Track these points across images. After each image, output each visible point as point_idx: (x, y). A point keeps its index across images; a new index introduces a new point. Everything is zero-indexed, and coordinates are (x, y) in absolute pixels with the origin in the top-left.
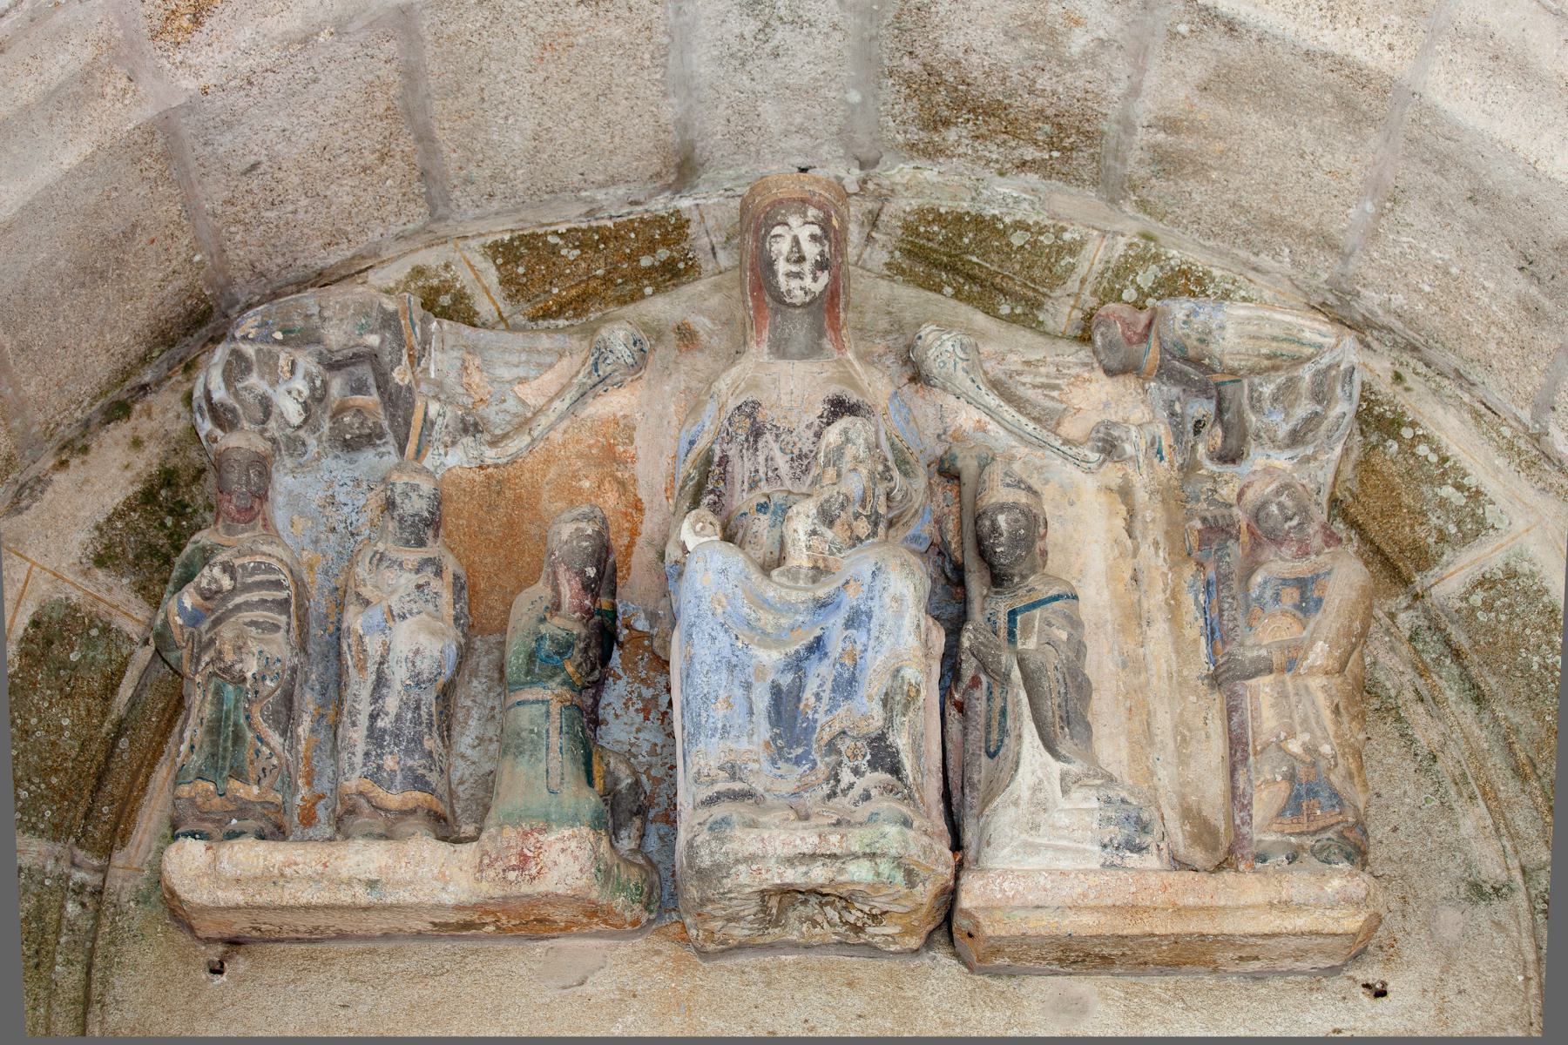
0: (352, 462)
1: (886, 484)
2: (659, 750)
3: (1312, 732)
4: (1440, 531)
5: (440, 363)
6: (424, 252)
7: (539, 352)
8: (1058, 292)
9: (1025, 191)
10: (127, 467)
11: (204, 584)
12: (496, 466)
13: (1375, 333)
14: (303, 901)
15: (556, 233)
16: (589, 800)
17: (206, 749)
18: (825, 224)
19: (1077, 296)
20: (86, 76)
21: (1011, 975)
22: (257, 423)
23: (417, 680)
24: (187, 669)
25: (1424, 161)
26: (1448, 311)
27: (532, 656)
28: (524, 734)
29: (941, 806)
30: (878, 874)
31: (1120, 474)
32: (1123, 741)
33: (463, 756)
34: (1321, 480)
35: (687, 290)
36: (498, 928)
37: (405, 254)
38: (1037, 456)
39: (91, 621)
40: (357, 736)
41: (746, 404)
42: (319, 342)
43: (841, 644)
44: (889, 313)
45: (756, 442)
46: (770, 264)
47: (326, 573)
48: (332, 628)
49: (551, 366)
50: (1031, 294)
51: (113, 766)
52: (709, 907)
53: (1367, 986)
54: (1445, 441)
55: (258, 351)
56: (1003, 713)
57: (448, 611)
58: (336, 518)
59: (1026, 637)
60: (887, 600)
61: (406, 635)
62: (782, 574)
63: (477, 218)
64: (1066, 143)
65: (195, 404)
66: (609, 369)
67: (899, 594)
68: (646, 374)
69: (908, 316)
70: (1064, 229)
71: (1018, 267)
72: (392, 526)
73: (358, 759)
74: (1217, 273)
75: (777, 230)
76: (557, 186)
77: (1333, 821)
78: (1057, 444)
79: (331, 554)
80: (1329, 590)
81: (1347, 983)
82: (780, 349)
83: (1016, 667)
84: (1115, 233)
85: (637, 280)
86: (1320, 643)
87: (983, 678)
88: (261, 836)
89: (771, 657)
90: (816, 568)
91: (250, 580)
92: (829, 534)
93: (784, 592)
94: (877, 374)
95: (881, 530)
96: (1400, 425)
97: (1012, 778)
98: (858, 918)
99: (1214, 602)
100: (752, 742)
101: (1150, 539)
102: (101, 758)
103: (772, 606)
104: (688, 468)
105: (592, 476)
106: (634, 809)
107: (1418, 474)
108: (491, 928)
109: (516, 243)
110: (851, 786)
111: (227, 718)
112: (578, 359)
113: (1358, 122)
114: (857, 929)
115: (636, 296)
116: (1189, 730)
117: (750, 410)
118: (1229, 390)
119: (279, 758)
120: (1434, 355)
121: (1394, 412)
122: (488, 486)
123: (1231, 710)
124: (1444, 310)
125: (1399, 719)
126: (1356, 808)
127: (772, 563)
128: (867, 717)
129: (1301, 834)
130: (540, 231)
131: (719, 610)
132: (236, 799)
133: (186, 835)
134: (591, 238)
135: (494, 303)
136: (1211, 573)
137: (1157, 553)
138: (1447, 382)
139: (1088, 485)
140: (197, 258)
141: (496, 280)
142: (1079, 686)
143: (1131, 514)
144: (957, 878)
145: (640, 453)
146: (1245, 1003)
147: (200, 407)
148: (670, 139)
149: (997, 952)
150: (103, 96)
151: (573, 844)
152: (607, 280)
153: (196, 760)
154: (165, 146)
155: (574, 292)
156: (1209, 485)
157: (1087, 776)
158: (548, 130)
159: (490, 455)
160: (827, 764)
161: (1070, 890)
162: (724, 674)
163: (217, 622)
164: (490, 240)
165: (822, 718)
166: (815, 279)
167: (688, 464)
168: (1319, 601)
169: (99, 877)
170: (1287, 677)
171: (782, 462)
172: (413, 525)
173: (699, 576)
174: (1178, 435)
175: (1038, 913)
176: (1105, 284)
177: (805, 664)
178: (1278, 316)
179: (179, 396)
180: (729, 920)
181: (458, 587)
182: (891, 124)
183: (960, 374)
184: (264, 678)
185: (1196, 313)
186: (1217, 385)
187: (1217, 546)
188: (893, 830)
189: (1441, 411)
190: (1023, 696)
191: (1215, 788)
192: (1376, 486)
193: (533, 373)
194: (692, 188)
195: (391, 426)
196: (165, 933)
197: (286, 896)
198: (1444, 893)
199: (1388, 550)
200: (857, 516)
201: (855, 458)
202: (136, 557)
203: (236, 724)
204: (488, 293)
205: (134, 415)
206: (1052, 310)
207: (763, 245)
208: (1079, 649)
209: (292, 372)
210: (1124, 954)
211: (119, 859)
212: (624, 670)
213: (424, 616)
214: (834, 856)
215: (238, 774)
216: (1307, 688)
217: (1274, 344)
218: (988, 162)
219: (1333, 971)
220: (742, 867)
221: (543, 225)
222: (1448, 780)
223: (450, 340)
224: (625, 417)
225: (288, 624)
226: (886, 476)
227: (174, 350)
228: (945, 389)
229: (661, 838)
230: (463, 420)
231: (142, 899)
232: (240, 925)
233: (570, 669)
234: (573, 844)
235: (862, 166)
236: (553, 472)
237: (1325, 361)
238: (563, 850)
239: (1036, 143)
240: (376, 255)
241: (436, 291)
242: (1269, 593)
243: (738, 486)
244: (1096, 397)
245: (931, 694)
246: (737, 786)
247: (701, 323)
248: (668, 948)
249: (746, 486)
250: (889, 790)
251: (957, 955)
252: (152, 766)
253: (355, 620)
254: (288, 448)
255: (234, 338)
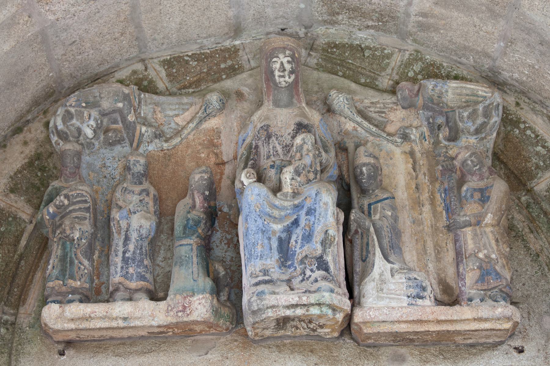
0: (112, 150)
1: (319, 158)
2: (234, 259)
3: (488, 250)
4: (537, 164)
5: (145, 110)
6: (136, 65)
7: (183, 104)
8: (383, 74)
9: (369, 35)
10: (22, 153)
11: (57, 203)
12: (168, 150)
13: (508, 87)
14: (98, 326)
15: (187, 55)
16: (209, 283)
17: (59, 267)
18: (293, 56)
19: (391, 75)
20: (13, 17)
21: (375, 347)
22: (75, 138)
23: (141, 237)
24: (51, 236)
25: (522, 30)
26: (535, 80)
27: (185, 227)
28: (183, 258)
29: (345, 282)
30: (322, 311)
31: (410, 146)
32: (414, 253)
33: (158, 265)
34: (488, 146)
35: (239, 77)
36: (173, 333)
37: (129, 65)
38: (377, 141)
39: (9, 215)
40: (118, 260)
41: (264, 126)
42: (99, 106)
43: (304, 221)
44: (318, 84)
45: (269, 140)
46: (272, 72)
47: (103, 194)
48: (106, 216)
49: (188, 109)
50: (373, 75)
51: (19, 272)
52: (257, 325)
53: (515, 348)
54: (537, 129)
55: (76, 111)
56: (368, 244)
57: (152, 209)
58: (106, 172)
59: (375, 214)
60: (322, 204)
61: (136, 222)
62: (281, 195)
63: (157, 51)
64: (384, 20)
65: (50, 130)
66: (210, 111)
67: (328, 198)
68: (224, 112)
69: (325, 85)
70: (385, 49)
71: (367, 64)
72: (129, 177)
73: (119, 269)
74: (445, 64)
75: (275, 59)
76: (188, 39)
77: (498, 284)
78: (385, 136)
79: (105, 187)
80: (492, 193)
81: (508, 347)
82: (277, 104)
83: (372, 226)
84: (405, 50)
85: (220, 73)
86: (490, 214)
87: (359, 230)
88: (81, 301)
89: (278, 227)
90: (294, 192)
91: (75, 200)
92: (299, 179)
93: (282, 202)
94: (314, 112)
95: (318, 176)
96: (519, 123)
97: (372, 270)
98: (314, 326)
99: (448, 197)
100: (272, 262)
101: (422, 172)
102: (14, 269)
103: (277, 207)
104: (242, 151)
105: (205, 152)
106: (227, 286)
107: (527, 142)
108: (171, 333)
109: (172, 60)
110: (310, 276)
111: (67, 255)
112: (198, 107)
113: (495, 16)
114: (314, 331)
115: (219, 80)
116: (440, 248)
117: (266, 128)
118: (450, 114)
119: (88, 270)
120: (532, 95)
121: (517, 118)
122: (165, 158)
123: (456, 241)
124: (534, 80)
125: (523, 240)
126: (506, 279)
127: (277, 189)
128: (315, 250)
129: (485, 290)
130: (181, 55)
131: (258, 210)
132: (71, 287)
133: (51, 302)
134: (201, 57)
135: (164, 84)
136: (446, 186)
137: (425, 178)
138: (537, 105)
139: (397, 151)
140: (51, 74)
141: (165, 75)
142: (397, 233)
143: (415, 162)
144: (352, 310)
145: (223, 142)
146: (467, 356)
147: (52, 131)
148: (232, 22)
149: (369, 338)
150: (19, 24)
151: (203, 301)
152: (208, 73)
153: (56, 272)
154: (43, 39)
155: (195, 79)
156: (444, 150)
157: (401, 269)
158: (185, 21)
159: (165, 145)
160: (301, 268)
161: (396, 315)
162: (260, 235)
163: (62, 217)
164: (162, 59)
165: (298, 251)
166: (290, 78)
167: (243, 149)
168: (489, 197)
169: (13, 317)
170: (477, 227)
171: (279, 148)
172: (138, 176)
173: (249, 197)
174: (432, 130)
175: (384, 324)
176: (401, 70)
177: (291, 229)
178: (469, 86)
179: (42, 124)
180: (264, 329)
181: (155, 199)
182: (317, 14)
183: (346, 109)
184: (81, 239)
185: (437, 86)
186: (446, 112)
187: (449, 178)
188: (327, 294)
189: (535, 117)
190: (375, 237)
191: (451, 271)
192: (511, 147)
193: (181, 113)
194: (240, 37)
195: (127, 136)
196: (41, 339)
197: (92, 325)
198: (545, 310)
199: (516, 172)
200: (309, 172)
201: (308, 150)
202: (27, 188)
203: (71, 258)
204: (162, 80)
205: (24, 132)
206: (381, 81)
207: (269, 65)
208: (396, 219)
209: (89, 118)
210: (418, 338)
211: (22, 310)
212: (220, 228)
213: (143, 212)
214: (304, 305)
215: (72, 277)
216: (485, 232)
217: (467, 97)
218: (354, 26)
219: (501, 343)
220: (270, 310)
221: (182, 53)
222: (544, 264)
223: (149, 101)
224: (217, 128)
225: (90, 216)
226: (319, 155)
227: (40, 107)
228: (340, 115)
229: (236, 294)
230: (155, 133)
231: (31, 326)
232: (72, 336)
233: (200, 231)
234: (203, 301)
235: (306, 28)
236: (189, 151)
237: (488, 102)
238: (200, 304)
239: (373, 20)
240: (118, 66)
241: (141, 80)
242: (469, 194)
243: (262, 157)
244: (397, 117)
245: (339, 239)
246: (267, 278)
247: (245, 90)
248: (240, 338)
249: (265, 157)
250: (325, 278)
251: (352, 339)
252: (34, 272)
253: (116, 215)
254: (87, 146)
255: (66, 106)
